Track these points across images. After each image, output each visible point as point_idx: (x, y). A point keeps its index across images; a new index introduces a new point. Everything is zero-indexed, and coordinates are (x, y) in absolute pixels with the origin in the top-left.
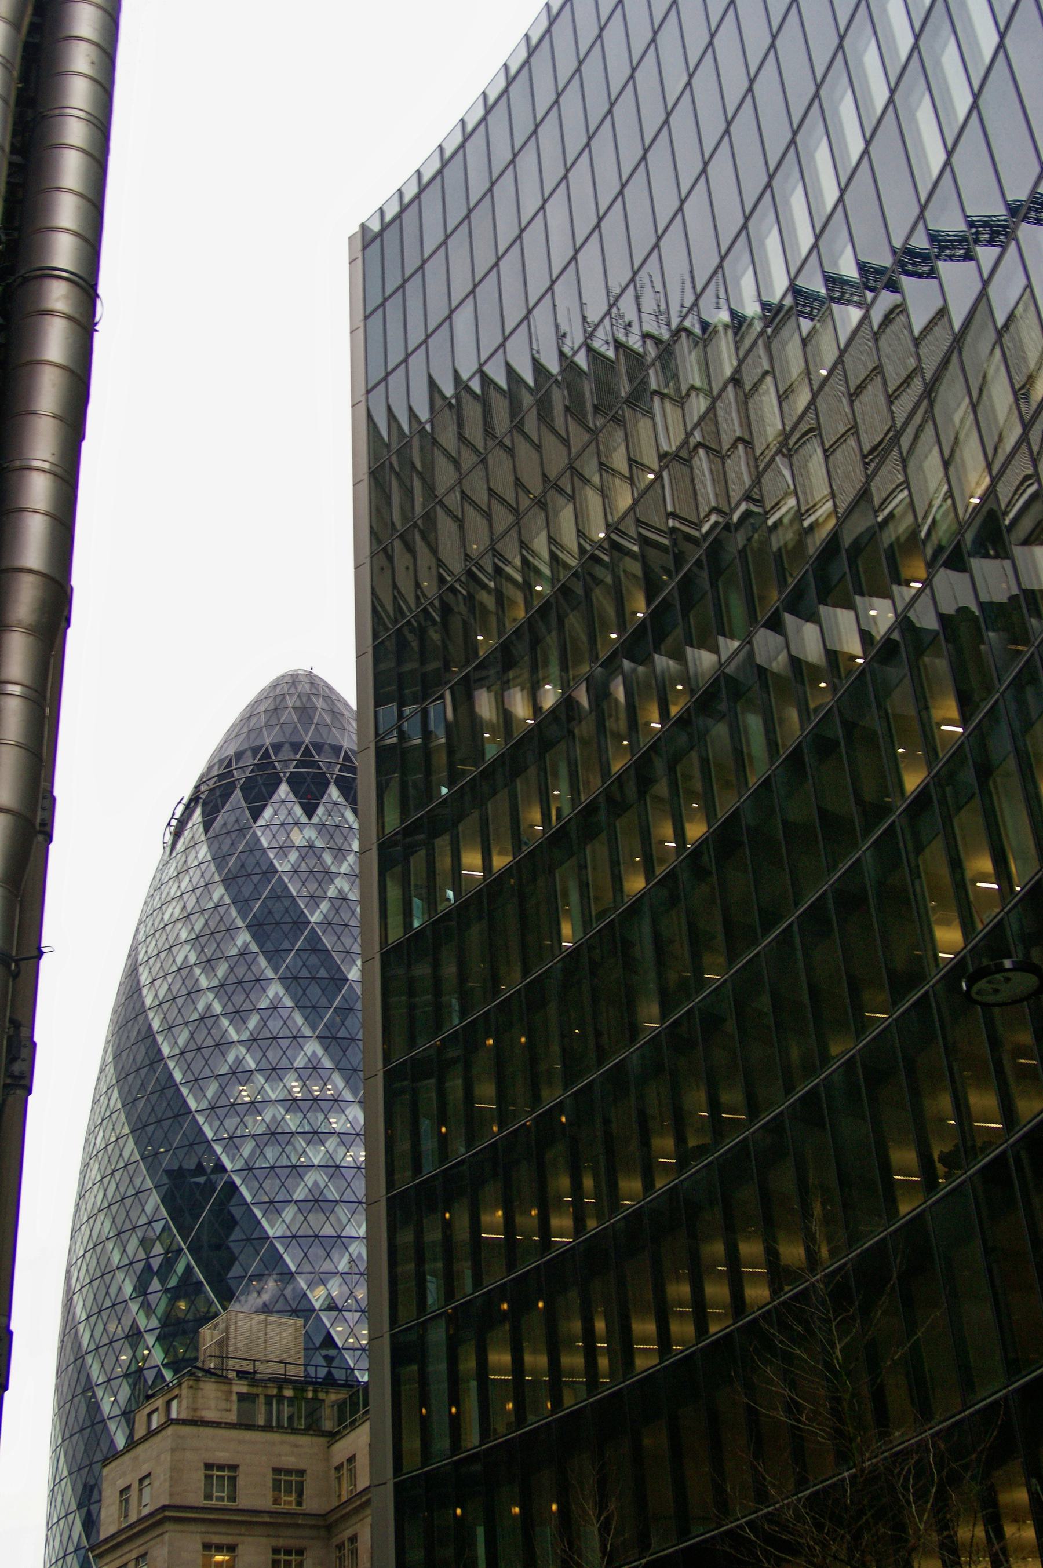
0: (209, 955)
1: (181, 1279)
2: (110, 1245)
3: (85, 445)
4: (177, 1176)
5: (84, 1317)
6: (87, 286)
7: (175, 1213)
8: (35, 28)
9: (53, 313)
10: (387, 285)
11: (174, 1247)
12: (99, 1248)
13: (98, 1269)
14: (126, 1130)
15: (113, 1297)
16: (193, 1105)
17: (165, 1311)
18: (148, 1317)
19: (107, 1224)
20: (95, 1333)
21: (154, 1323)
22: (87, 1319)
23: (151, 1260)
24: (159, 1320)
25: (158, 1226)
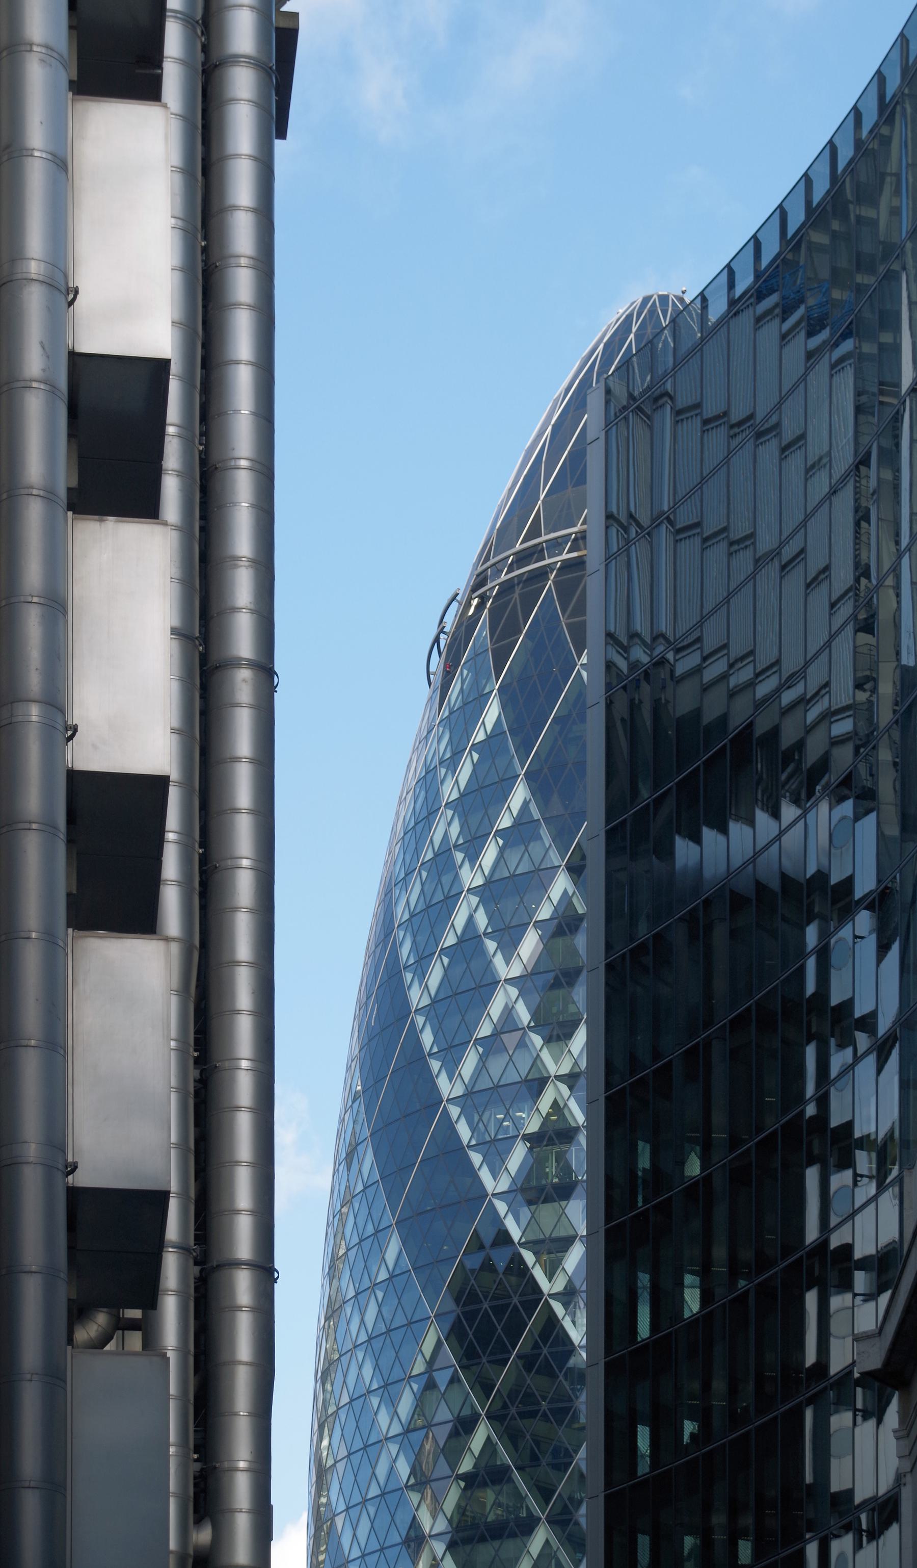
0: (496, 1076)
1: (478, 1460)
2: (375, 1401)
3: (274, 1545)
4: (465, 1295)
5: (351, 1293)
6: (265, 670)
7: (468, 1357)
8: (204, 860)
9: (240, 1363)
10: (827, 659)
11: (466, 1412)
12: (358, 1404)
13: (363, 1331)
14: (389, 1219)
15: (382, 1481)
16: (544, 1284)
17: (458, 1506)
18: (434, 1517)
19: (368, 1371)
20: (358, 1533)
21: (442, 1525)
22: (359, 1243)
23: (434, 1373)
24: (450, 1521)
25: (442, 1379)
